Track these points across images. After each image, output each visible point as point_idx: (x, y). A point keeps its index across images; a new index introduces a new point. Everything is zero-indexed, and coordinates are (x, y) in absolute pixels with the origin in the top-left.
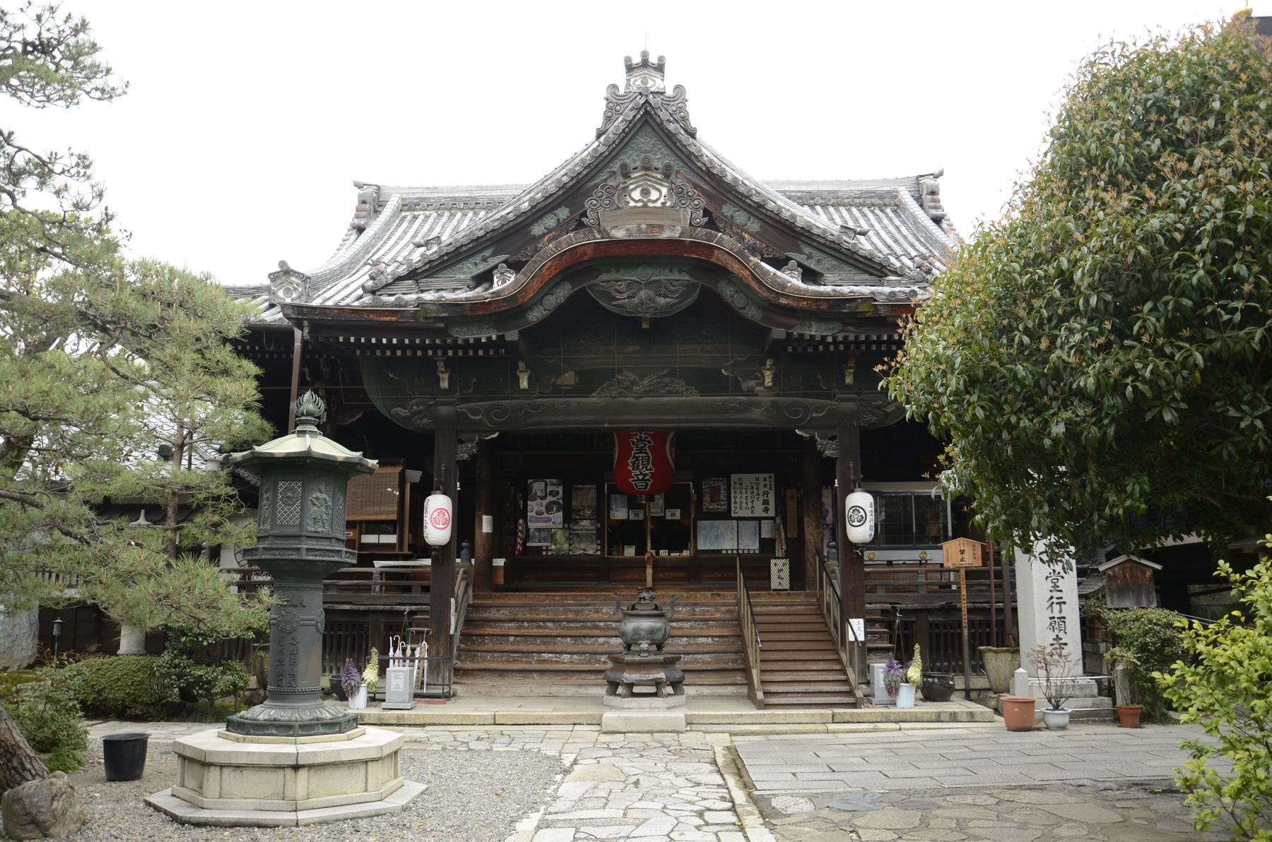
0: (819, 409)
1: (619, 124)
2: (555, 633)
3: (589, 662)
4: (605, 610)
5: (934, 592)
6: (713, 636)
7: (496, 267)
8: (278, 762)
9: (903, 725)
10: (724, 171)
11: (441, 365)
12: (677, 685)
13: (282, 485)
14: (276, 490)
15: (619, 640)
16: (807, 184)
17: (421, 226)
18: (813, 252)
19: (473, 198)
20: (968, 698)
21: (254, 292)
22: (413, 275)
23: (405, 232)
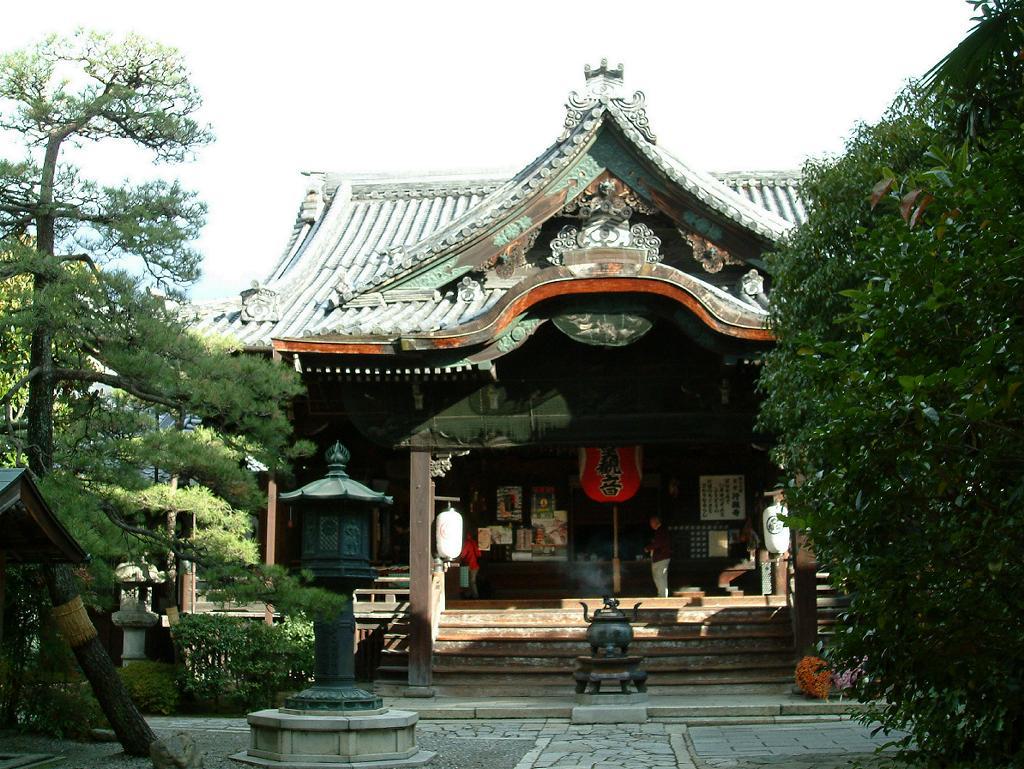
13: (323, 520)
14: (318, 524)
19: (426, 185)
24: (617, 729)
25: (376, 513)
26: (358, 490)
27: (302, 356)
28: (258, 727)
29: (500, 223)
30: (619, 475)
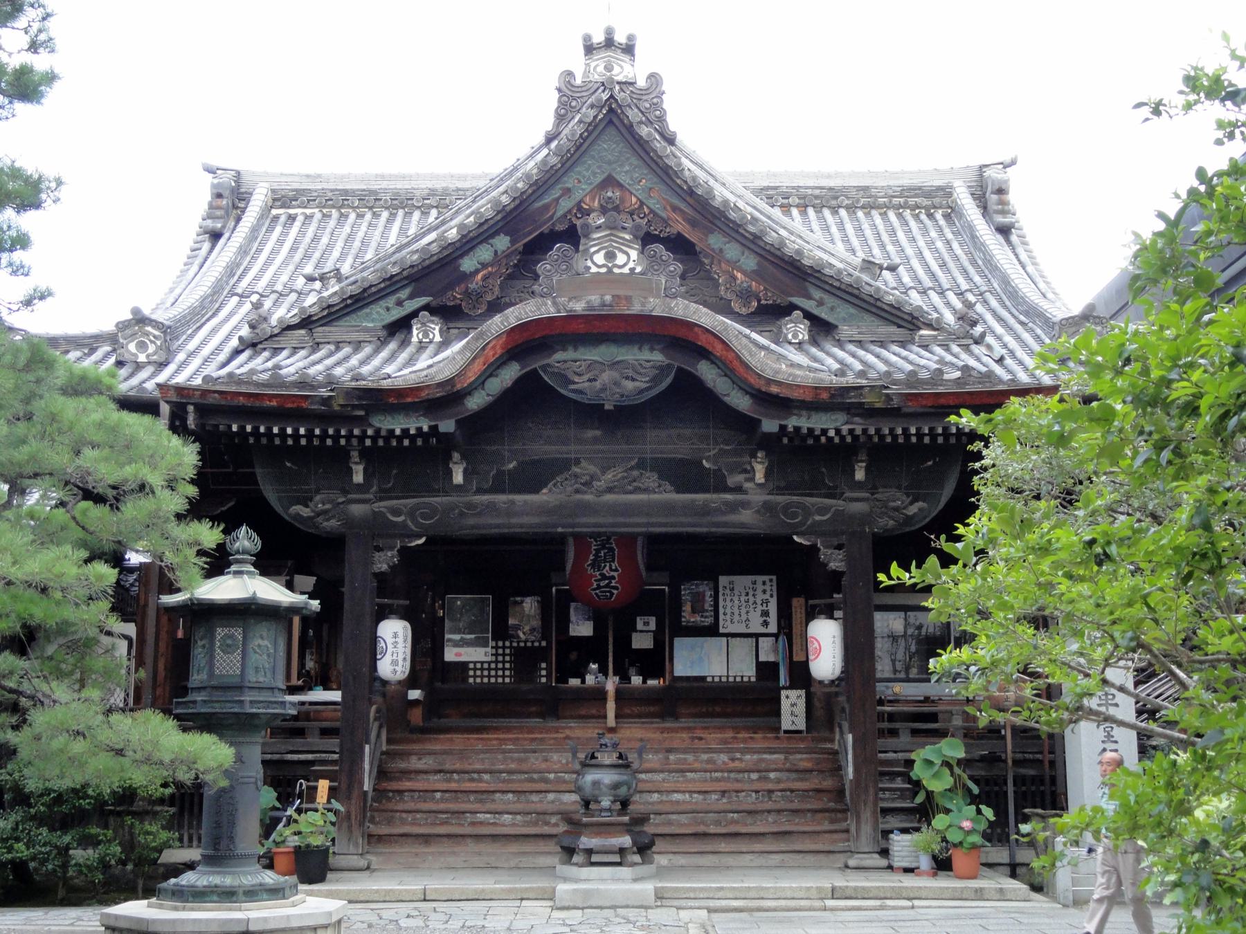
0: (822, 510)
1: (573, 128)
2: (492, 787)
3: (536, 824)
4: (555, 757)
6: (691, 792)
7: (414, 314)
9: (916, 903)
10: (710, 190)
11: (355, 455)
12: (644, 849)
13: (220, 632)
15: (574, 797)
16: (829, 176)
17: (302, 233)
18: (826, 297)
21: (89, 343)
23: (280, 242)
24: (617, 916)
25: (296, 620)
26: (271, 591)
27: (365, 454)
29: (468, 243)
30: (615, 574)
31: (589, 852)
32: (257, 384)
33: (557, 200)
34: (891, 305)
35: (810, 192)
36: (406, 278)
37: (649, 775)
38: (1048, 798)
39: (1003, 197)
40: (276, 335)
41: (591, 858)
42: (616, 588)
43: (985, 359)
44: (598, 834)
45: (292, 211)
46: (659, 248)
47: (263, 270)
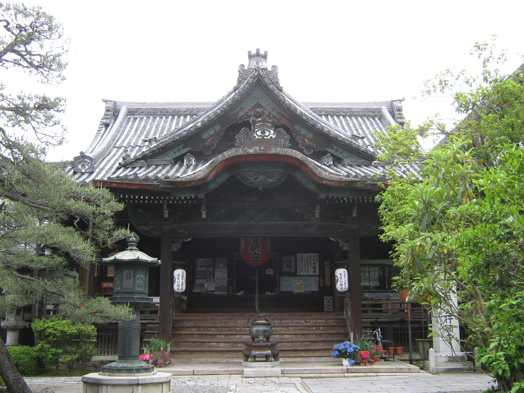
2: (216, 333)
3: (233, 347)
5: (396, 313)
6: (291, 334)
7: (185, 154)
8: (130, 383)
9: (378, 374)
10: (296, 109)
11: (165, 207)
13: (125, 272)
14: (123, 274)
15: (250, 337)
16: (336, 104)
17: (139, 124)
19: (166, 109)
20: (411, 363)
22: (145, 157)
23: (131, 128)
26: (144, 257)
27: (169, 207)
28: (88, 383)
29: (206, 127)
30: (260, 252)
31: (255, 357)
32: (130, 180)
33: (238, 112)
34: (363, 152)
35: (329, 110)
36: (182, 141)
37: (275, 328)
38: (423, 336)
39: (401, 112)
40: (133, 162)
41: (255, 358)
42: (260, 258)
43: (399, 171)
44: (258, 350)
45: (135, 116)
46: (282, 130)
47: (125, 138)
